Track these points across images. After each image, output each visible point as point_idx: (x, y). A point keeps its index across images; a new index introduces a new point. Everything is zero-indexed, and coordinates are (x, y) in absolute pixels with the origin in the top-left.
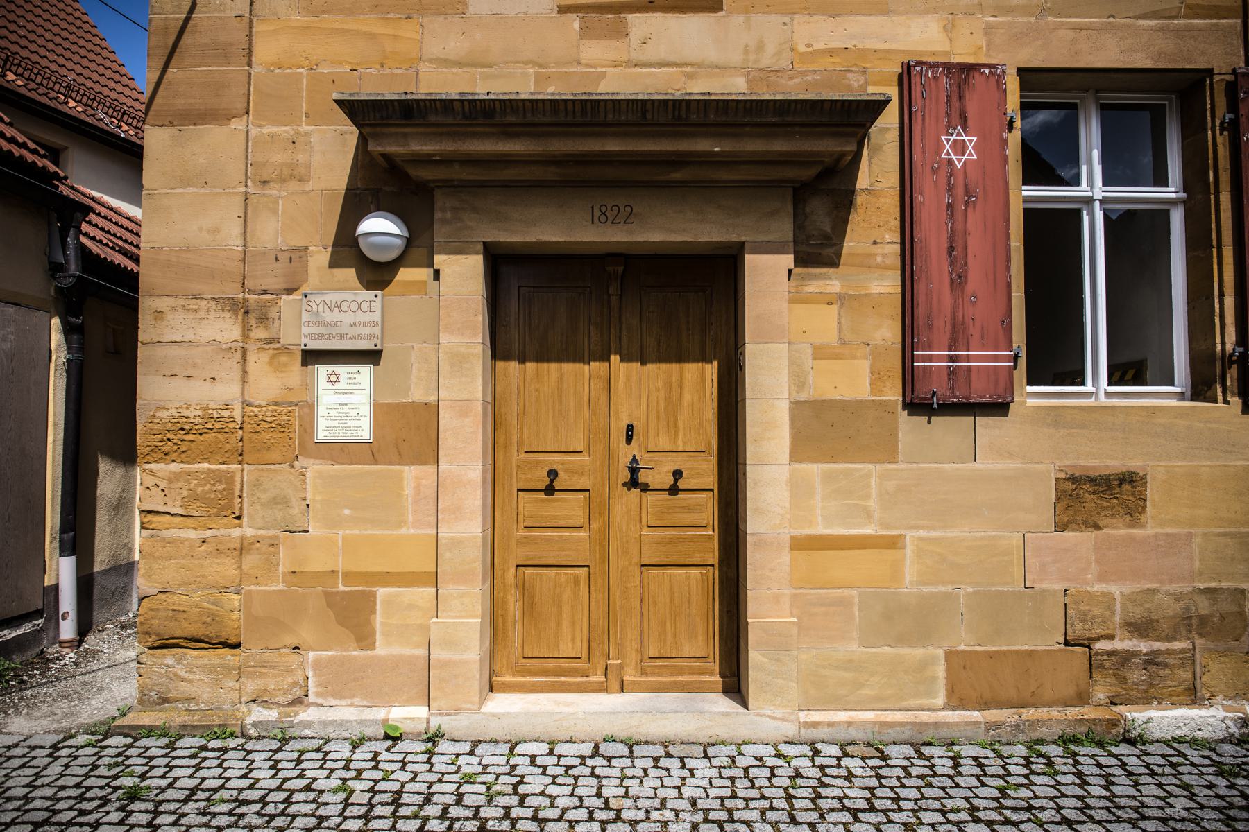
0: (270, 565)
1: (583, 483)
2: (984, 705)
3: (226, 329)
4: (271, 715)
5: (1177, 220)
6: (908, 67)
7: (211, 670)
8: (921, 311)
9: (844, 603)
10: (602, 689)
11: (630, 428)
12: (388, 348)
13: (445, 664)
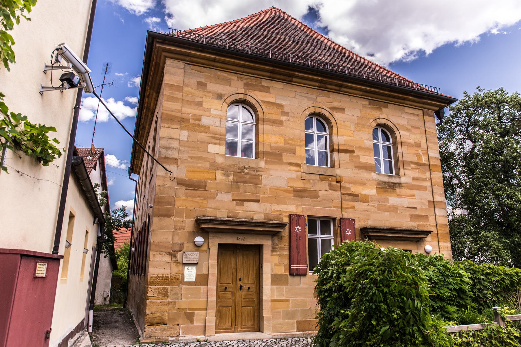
0: (174, 307)
1: (231, 290)
2: (303, 331)
3: (168, 258)
4: (174, 339)
5: (332, 241)
6: (290, 215)
7: (161, 330)
8: (292, 258)
9: (279, 312)
10: (234, 332)
11: (240, 278)
12: (199, 263)
13: (209, 326)
